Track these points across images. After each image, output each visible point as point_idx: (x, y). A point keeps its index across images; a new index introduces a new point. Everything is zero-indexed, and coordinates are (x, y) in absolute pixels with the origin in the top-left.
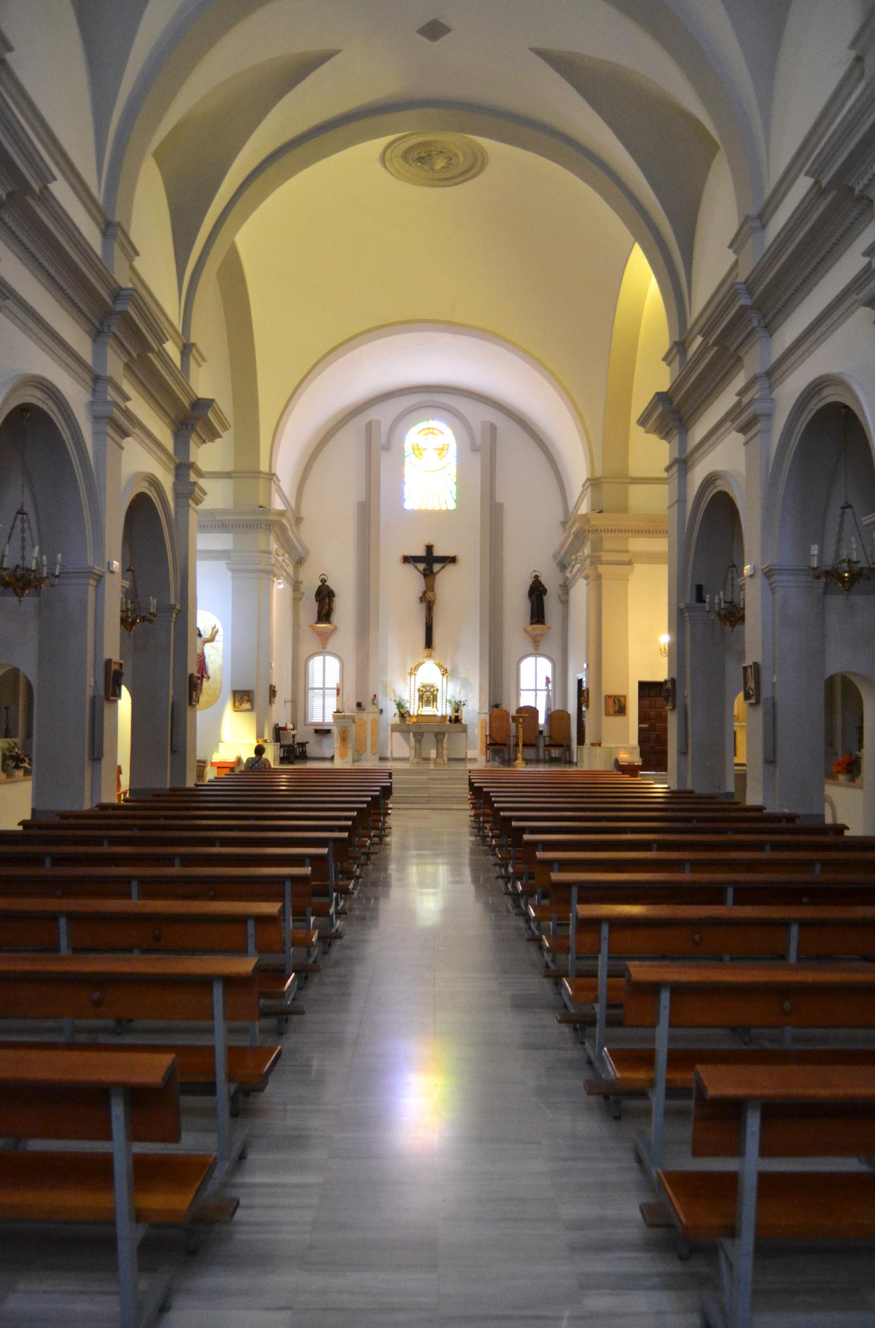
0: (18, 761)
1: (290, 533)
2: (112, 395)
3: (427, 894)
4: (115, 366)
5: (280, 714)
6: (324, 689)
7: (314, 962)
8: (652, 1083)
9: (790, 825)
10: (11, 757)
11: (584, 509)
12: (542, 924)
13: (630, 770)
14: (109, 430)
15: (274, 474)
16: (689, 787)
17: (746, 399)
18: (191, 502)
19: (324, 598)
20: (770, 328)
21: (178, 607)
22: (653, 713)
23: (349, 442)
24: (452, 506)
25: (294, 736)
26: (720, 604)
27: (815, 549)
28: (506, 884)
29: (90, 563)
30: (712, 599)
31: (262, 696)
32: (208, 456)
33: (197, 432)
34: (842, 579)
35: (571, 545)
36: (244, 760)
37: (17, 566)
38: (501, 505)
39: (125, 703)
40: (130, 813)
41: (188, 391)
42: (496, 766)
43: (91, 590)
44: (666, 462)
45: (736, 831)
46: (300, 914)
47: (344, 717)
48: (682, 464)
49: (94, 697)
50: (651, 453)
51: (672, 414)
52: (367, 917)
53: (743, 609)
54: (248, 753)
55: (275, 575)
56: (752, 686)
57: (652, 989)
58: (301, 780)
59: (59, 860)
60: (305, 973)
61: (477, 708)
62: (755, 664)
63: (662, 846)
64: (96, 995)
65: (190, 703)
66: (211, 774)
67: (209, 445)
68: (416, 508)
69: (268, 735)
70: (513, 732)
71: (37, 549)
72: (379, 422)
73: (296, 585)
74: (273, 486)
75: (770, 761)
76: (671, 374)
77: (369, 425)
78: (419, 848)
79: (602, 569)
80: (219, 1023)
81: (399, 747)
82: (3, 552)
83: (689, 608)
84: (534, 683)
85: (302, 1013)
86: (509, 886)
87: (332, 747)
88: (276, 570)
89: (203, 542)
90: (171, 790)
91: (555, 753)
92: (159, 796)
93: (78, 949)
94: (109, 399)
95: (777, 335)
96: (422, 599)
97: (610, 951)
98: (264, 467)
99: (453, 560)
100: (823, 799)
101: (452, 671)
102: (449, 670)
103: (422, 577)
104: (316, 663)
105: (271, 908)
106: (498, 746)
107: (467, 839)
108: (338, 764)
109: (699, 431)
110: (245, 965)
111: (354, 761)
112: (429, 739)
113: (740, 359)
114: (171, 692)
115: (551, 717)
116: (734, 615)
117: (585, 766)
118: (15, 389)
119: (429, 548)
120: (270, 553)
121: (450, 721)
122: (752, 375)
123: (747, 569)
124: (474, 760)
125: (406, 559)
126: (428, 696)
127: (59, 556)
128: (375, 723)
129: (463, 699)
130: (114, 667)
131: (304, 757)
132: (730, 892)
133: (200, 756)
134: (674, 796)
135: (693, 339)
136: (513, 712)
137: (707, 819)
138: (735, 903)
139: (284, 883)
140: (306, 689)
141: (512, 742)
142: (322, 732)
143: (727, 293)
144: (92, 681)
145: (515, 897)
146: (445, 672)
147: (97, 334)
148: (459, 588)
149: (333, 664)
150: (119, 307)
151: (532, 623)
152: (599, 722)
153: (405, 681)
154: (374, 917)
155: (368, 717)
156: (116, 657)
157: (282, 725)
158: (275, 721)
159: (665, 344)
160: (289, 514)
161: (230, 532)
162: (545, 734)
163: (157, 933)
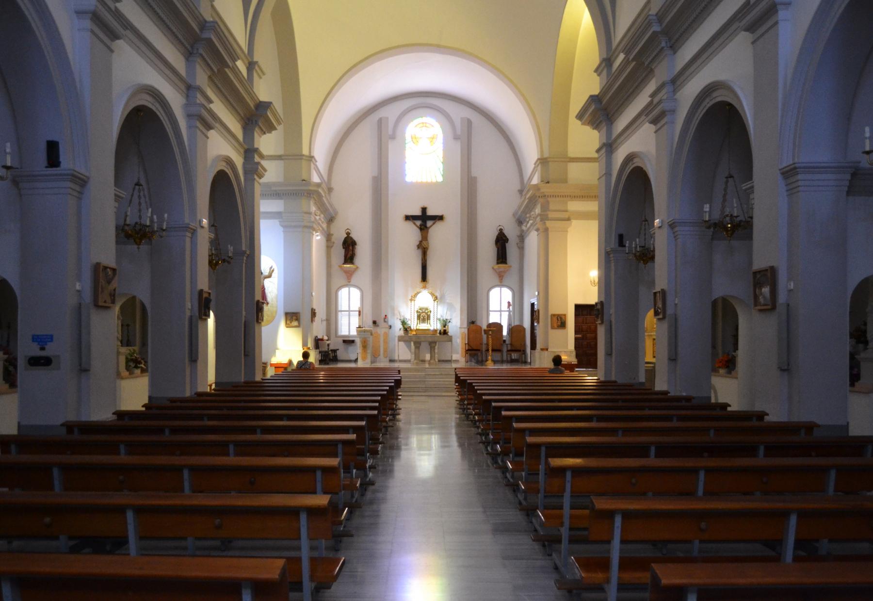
0: (137, 362)
1: (324, 199)
2: (200, 99)
3: (424, 455)
4: (202, 78)
5: (319, 329)
6: (349, 311)
7: (356, 501)
8: (608, 581)
9: (688, 404)
10: (132, 360)
11: (535, 181)
12: (516, 474)
13: (570, 367)
14: (198, 124)
15: (313, 157)
16: (613, 378)
17: (656, 100)
18: (256, 177)
19: (349, 246)
20: (674, 47)
21: (248, 253)
22: (585, 327)
23: (365, 134)
24: (440, 179)
25: (328, 345)
26: (636, 247)
27: (707, 208)
28: (486, 447)
29: (187, 221)
30: (631, 244)
31: (306, 316)
32: (268, 143)
33: (260, 128)
34: (726, 228)
35: (527, 206)
36: (295, 363)
37: (136, 223)
38: (475, 178)
39: (211, 321)
40: (218, 398)
41: (252, 95)
42: (473, 364)
43: (188, 240)
44: (597, 146)
45: (651, 408)
46: (347, 469)
47: (365, 331)
48: (608, 147)
49: (191, 316)
50: (585, 139)
51: (601, 111)
52: (388, 472)
53: (654, 251)
54: (297, 358)
55: (314, 230)
56: (660, 306)
57: (609, 515)
58: (333, 375)
59: (174, 431)
60: (354, 508)
61: (459, 324)
62: (662, 290)
63: (600, 419)
64: (217, 521)
65: (257, 321)
66: (270, 372)
67: (268, 135)
68: (414, 181)
69: (310, 344)
70: (485, 341)
71: (150, 210)
72: (387, 118)
73: (329, 237)
74: (312, 166)
75: (673, 359)
76: (601, 83)
77: (380, 121)
78: (417, 423)
79: (549, 224)
80: (305, 542)
81: (403, 352)
82: (126, 213)
83: (613, 251)
84: (499, 306)
85: (352, 536)
86: (489, 449)
87: (355, 352)
88: (315, 226)
89: (265, 206)
90: (245, 382)
91: (514, 356)
92: (237, 387)
93: (195, 490)
94: (198, 102)
95: (679, 53)
96: (419, 247)
97: (572, 492)
98: (305, 151)
99: (441, 218)
100: (711, 387)
101: (441, 298)
102: (439, 297)
103: (418, 230)
104: (343, 293)
105: (334, 462)
106: (473, 351)
107: (453, 417)
108: (360, 364)
109: (621, 123)
110: (321, 500)
111: (372, 362)
112: (425, 346)
113: (652, 71)
114: (244, 313)
115: (511, 330)
116: (647, 256)
117: (537, 365)
118: (134, 95)
119: (424, 210)
120: (310, 213)
121: (440, 333)
122: (659, 84)
123: (657, 221)
124: (457, 361)
125: (408, 218)
126: (424, 315)
127: (166, 215)
128: (386, 335)
129: (449, 318)
130: (205, 295)
131: (335, 360)
132: (653, 449)
133: (264, 360)
134: (602, 385)
135: (617, 56)
136: (484, 327)
137: (627, 401)
138: (656, 457)
139: (337, 445)
140: (337, 311)
141: (484, 348)
142: (348, 342)
143: (642, 23)
144: (190, 305)
145: (494, 456)
146: (436, 299)
147: (189, 55)
148: (445, 238)
149: (355, 293)
150: (205, 35)
151: (498, 263)
152: (546, 333)
153: (407, 305)
154: (392, 471)
155: (381, 331)
156: (206, 288)
157: (320, 337)
158: (315, 334)
159: (595, 60)
160: (324, 186)
161: (281, 199)
162: (507, 342)
163: (254, 479)
